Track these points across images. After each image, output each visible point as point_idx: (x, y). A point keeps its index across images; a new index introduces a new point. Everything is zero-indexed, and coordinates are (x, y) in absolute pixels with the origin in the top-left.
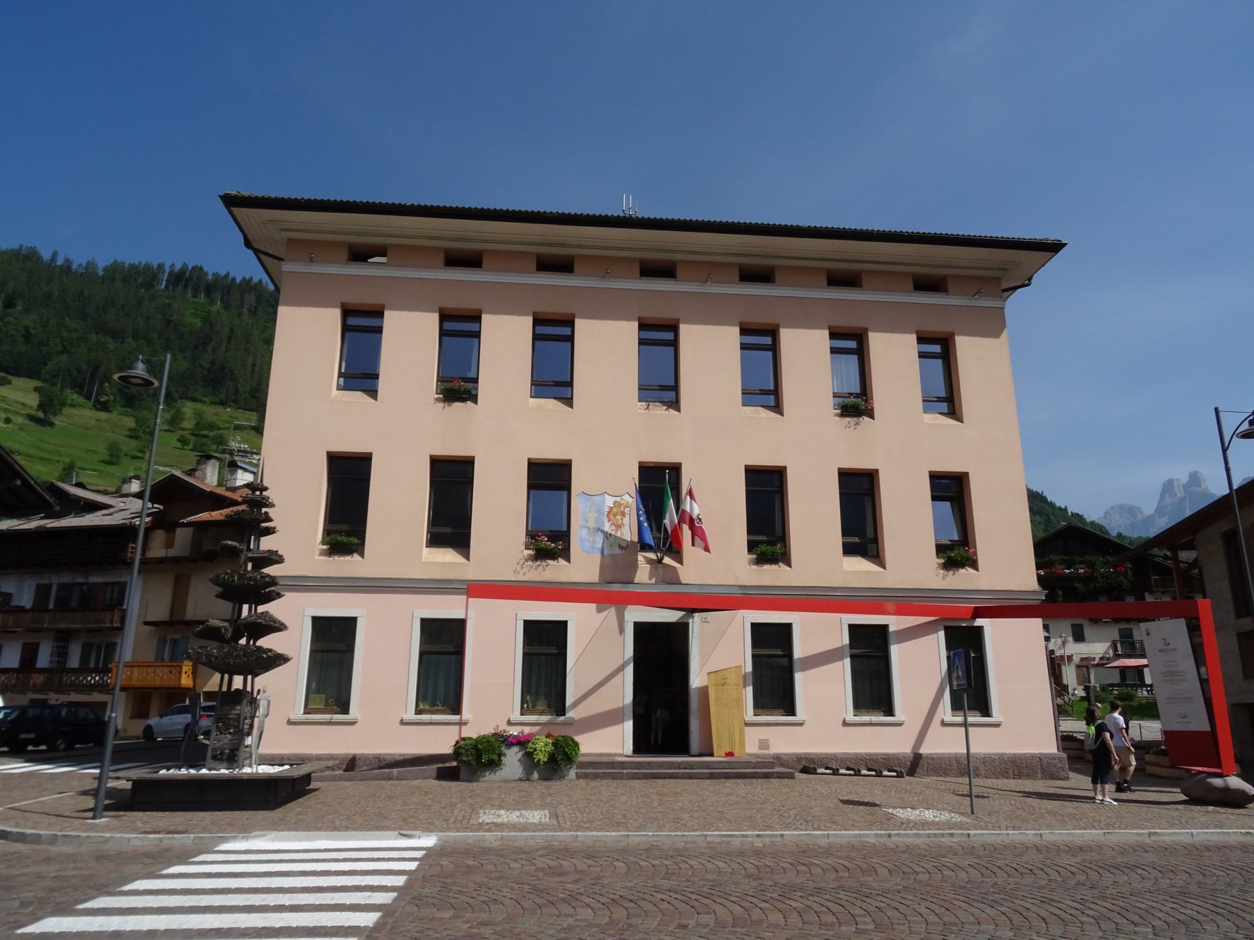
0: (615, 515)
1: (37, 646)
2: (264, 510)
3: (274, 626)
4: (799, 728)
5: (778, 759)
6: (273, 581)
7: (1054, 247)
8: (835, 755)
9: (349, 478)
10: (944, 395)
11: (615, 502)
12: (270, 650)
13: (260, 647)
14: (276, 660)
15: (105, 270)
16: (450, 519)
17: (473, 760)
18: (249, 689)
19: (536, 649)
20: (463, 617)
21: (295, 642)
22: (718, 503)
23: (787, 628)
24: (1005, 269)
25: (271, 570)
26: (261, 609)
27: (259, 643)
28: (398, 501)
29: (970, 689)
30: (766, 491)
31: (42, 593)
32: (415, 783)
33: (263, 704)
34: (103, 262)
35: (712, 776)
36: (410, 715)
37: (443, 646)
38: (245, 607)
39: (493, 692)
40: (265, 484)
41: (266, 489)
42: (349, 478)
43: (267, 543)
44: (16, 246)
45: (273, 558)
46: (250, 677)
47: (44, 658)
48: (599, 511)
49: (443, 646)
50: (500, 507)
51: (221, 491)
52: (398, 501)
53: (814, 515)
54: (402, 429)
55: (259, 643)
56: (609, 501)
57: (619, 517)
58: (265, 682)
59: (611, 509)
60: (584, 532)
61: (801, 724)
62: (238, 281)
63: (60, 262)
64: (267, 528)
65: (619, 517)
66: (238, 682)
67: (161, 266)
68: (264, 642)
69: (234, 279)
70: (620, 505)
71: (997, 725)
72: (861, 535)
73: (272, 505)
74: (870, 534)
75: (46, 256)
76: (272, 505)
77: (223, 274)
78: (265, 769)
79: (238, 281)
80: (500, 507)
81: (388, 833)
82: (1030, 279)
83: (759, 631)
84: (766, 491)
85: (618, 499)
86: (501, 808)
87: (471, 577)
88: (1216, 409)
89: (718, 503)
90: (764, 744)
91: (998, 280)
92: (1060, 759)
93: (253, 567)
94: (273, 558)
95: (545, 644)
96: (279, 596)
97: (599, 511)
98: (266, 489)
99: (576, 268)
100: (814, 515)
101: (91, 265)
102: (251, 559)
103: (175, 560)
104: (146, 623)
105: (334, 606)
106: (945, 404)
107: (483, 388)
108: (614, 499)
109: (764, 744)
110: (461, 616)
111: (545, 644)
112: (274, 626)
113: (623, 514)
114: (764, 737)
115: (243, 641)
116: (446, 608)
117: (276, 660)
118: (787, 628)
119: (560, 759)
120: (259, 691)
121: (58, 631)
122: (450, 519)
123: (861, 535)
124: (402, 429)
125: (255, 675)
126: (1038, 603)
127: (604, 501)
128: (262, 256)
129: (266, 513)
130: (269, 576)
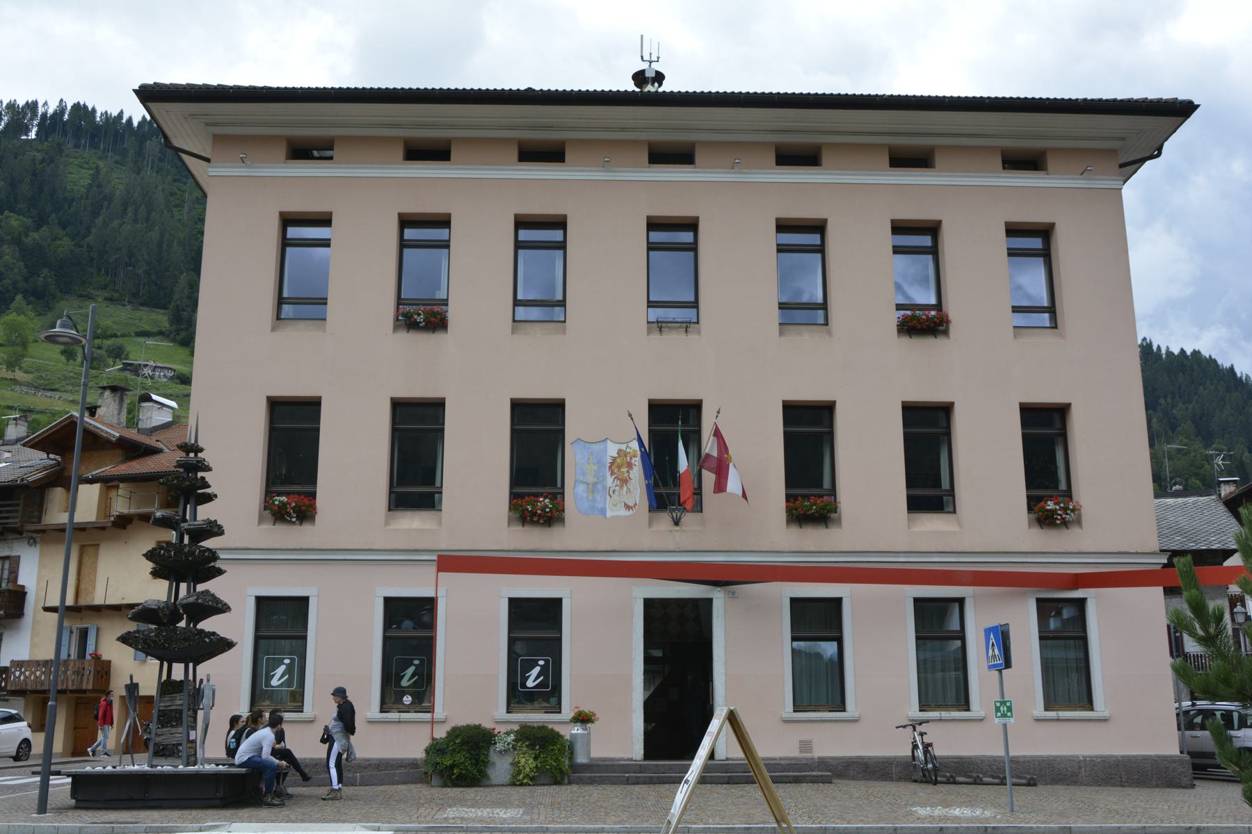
0: (619, 467)
2: (200, 474)
4: (853, 725)
5: (823, 763)
7: (1183, 110)
8: (895, 758)
9: (293, 433)
10: (1046, 304)
11: (620, 451)
12: (214, 634)
13: (202, 631)
14: (225, 645)
16: (415, 473)
17: (461, 760)
18: (191, 677)
19: (918, 492)
20: (432, 594)
21: (237, 625)
23: (837, 603)
24: (1123, 139)
25: (209, 543)
26: (201, 587)
27: (200, 626)
28: (353, 456)
30: (809, 433)
33: (208, 693)
35: (730, 781)
36: (1039, 711)
37: (409, 632)
38: (183, 586)
39: (471, 676)
40: (201, 444)
41: (201, 450)
42: (293, 433)
43: (205, 512)
45: (214, 529)
46: (191, 665)
48: (600, 463)
50: (476, 459)
52: (353, 456)
53: (869, 461)
54: (357, 374)
55: (200, 626)
56: (612, 450)
57: (624, 470)
59: (614, 459)
60: (581, 489)
61: (856, 721)
62: (135, 124)
64: (204, 494)
65: (624, 470)
67: (32, 106)
68: (207, 625)
69: (130, 120)
70: (626, 454)
71: (1105, 720)
72: (929, 487)
73: (208, 469)
77: (115, 113)
78: (207, 767)
80: (476, 459)
81: (346, 825)
82: (1160, 149)
84: (809, 433)
85: (623, 447)
86: (472, 806)
87: (443, 547)
91: (1112, 152)
92: (1181, 762)
94: (214, 529)
95: (535, 626)
96: (220, 572)
97: (600, 463)
98: (201, 450)
100: (869, 461)
102: (189, 532)
106: (1047, 315)
107: (454, 314)
108: (618, 447)
111: (535, 626)
113: (630, 465)
114: (806, 737)
115: (182, 624)
116: (413, 584)
117: (225, 645)
118: (837, 603)
120: (201, 681)
122: (415, 473)
123: (929, 487)
124: (357, 374)
126: (1159, 567)
127: (605, 449)
129: (203, 478)
130: (208, 550)
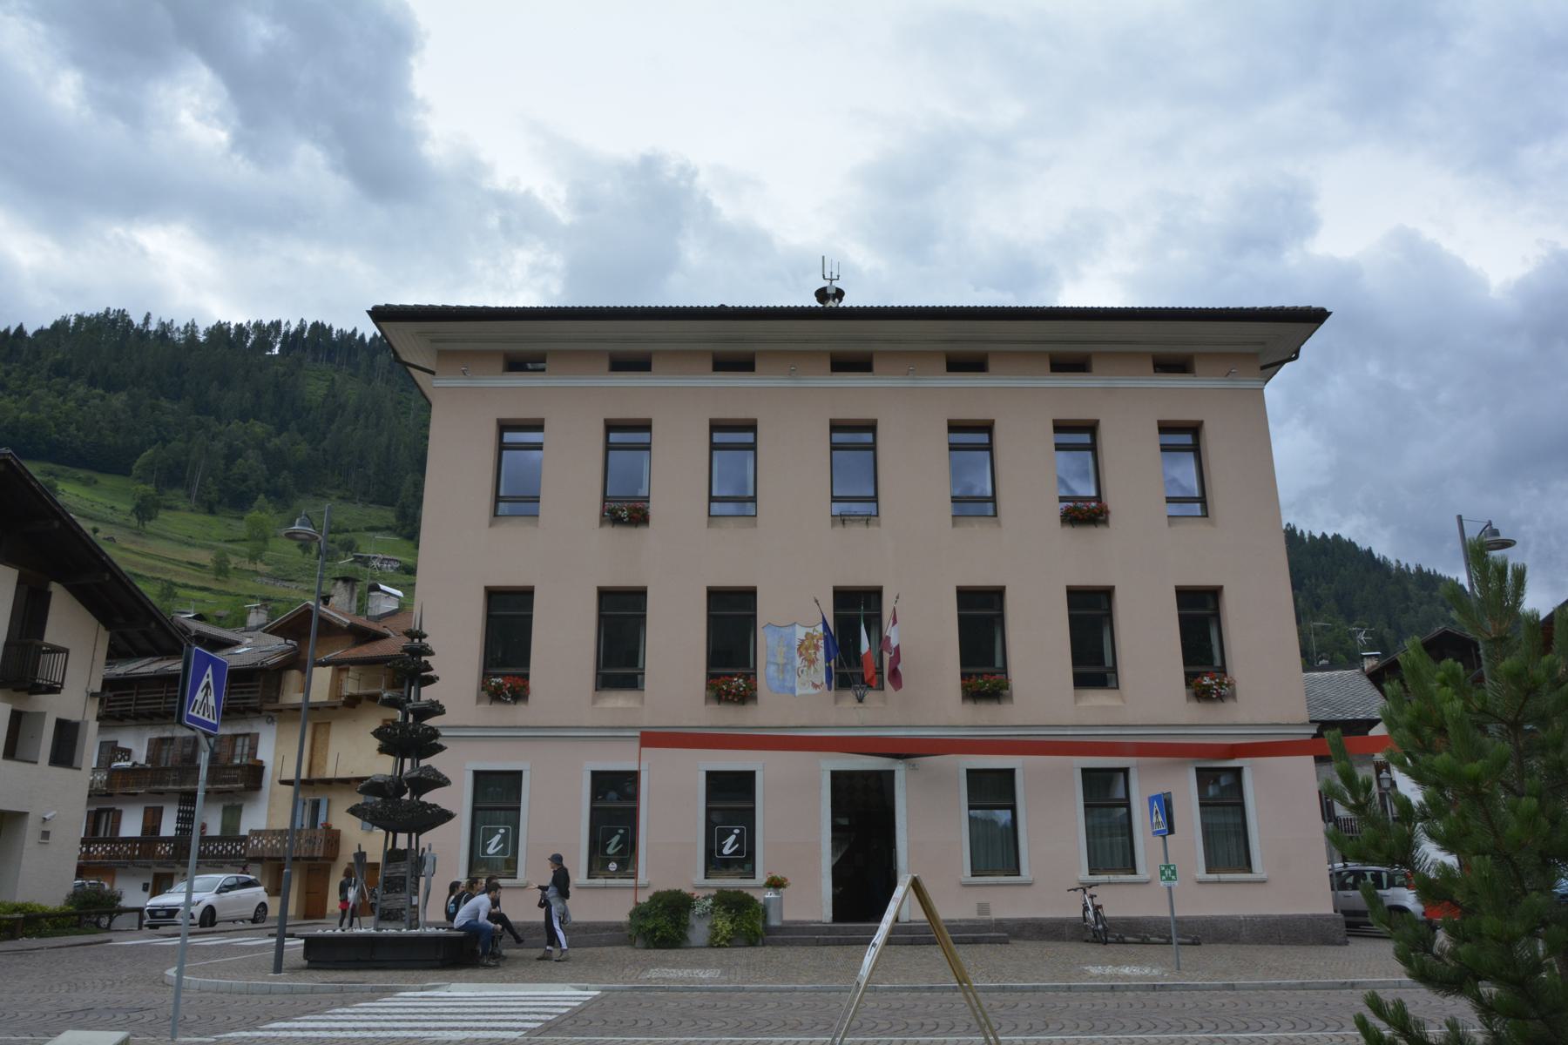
1: (160, 810)
3: (439, 781)
5: (1000, 925)
6: (434, 733)
8: (1067, 920)
9: (508, 619)
12: (435, 806)
14: (445, 816)
15: (209, 332)
21: (457, 797)
22: (924, 632)
23: (1011, 773)
25: (431, 722)
26: (423, 763)
27: (422, 799)
28: (564, 641)
29: (1228, 845)
30: (981, 615)
31: (157, 746)
32: (589, 950)
33: (429, 860)
34: (204, 325)
37: (614, 799)
38: (408, 762)
40: (425, 630)
42: (508, 619)
43: (428, 693)
44: (102, 311)
45: (435, 709)
47: (168, 828)
49: (614, 799)
50: (676, 642)
51: (362, 621)
52: (564, 641)
53: (1037, 642)
55: (422, 799)
56: (800, 633)
58: (430, 840)
60: (772, 669)
62: (367, 340)
63: (153, 327)
66: (402, 841)
68: (428, 798)
69: (363, 336)
70: (813, 637)
72: (1093, 662)
73: (431, 653)
74: (1108, 662)
75: (137, 320)
76: (431, 653)
77: (349, 331)
78: (430, 931)
79: (367, 340)
80: (676, 642)
82: (1297, 352)
83: (976, 778)
88: (1460, 518)
89: (924, 632)
90: (983, 908)
91: (1255, 356)
92: (1335, 919)
93: (415, 719)
94: (435, 709)
95: (731, 797)
96: (441, 748)
99: (757, 367)
100: (1037, 642)
101: (191, 329)
102: (413, 711)
103: (315, 708)
104: (283, 782)
105: (498, 760)
109: (983, 908)
110: (634, 767)
111: (731, 797)
112: (439, 781)
115: (406, 797)
116: (618, 760)
117: (445, 816)
119: (746, 924)
121: (183, 793)
123: (1093, 662)
125: (419, 833)
127: (794, 633)
128: (413, 371)
